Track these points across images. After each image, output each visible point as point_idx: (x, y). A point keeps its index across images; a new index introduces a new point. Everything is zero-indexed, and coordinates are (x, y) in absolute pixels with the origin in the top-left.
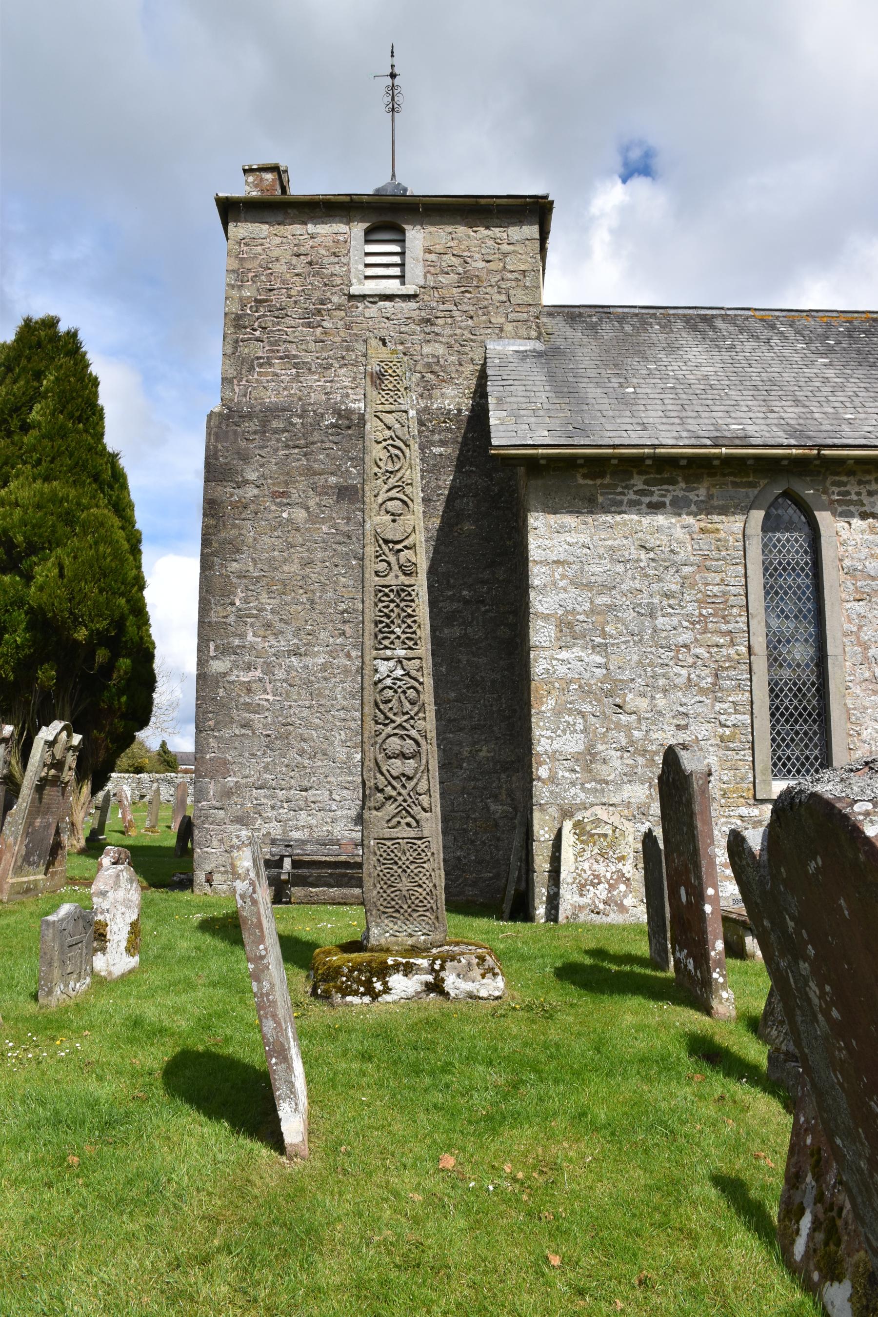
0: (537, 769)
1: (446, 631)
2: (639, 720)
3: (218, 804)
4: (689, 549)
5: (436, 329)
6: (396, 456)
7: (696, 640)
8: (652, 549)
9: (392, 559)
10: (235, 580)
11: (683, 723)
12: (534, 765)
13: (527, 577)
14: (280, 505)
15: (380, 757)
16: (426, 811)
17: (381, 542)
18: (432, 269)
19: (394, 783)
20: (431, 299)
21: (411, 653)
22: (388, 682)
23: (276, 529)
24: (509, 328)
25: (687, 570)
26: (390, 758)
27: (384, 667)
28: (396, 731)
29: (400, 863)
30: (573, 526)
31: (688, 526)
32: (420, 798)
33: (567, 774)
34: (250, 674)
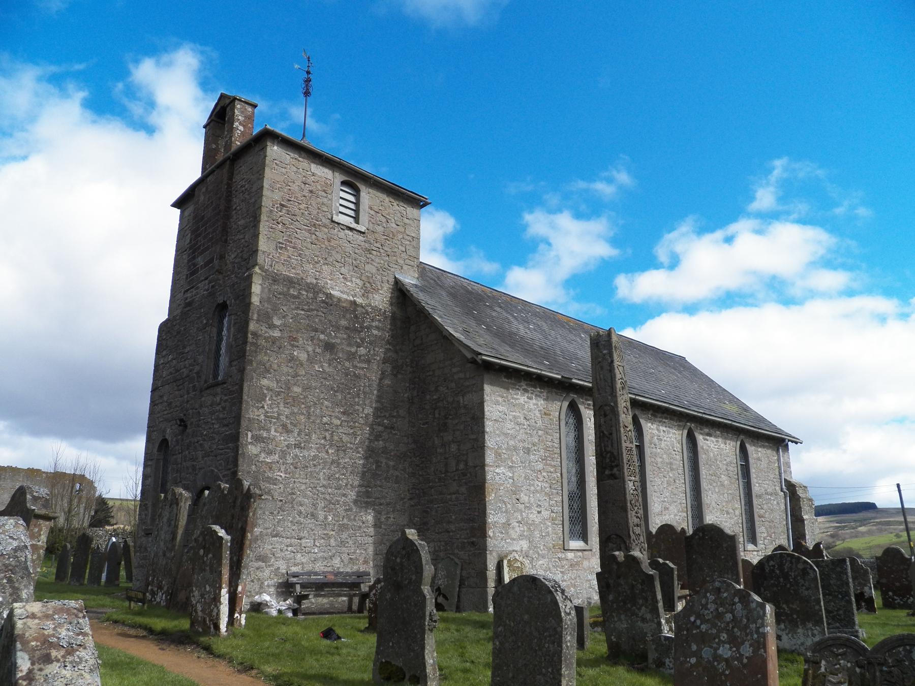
5: (373, 258)
10: (265, 392)
13: (484, 427)
14: (293, 346)
20: (371, 237)
23: (290, 361)
24: (405, 267)
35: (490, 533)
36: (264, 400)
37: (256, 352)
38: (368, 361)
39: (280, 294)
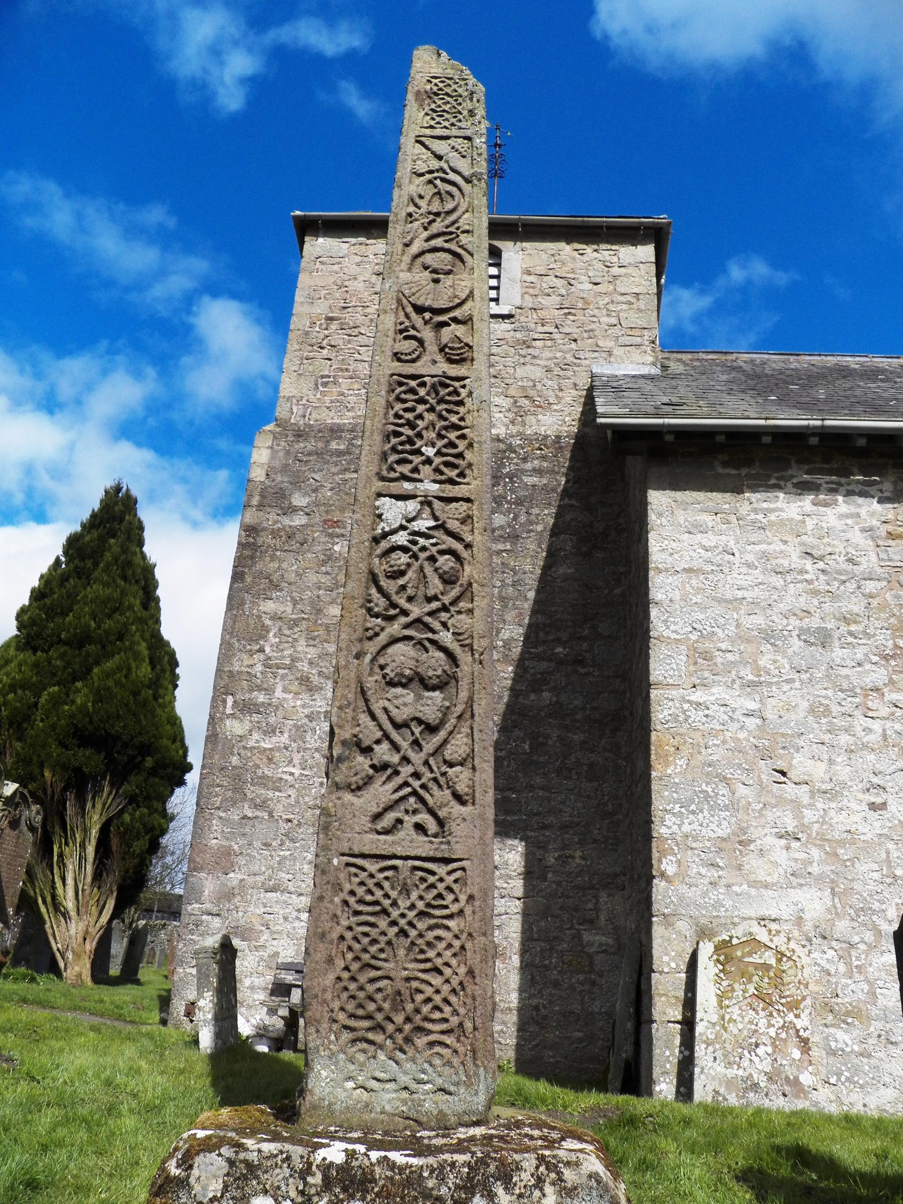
0: (660, 861)
1: (533, 696)
2: (812, 794)
3: (215, 910)
4: (874, 558)
5: (535, 352)
6: (448, 193)
7: (892, 682)
8: (821, 558)
9: (427, 334)
11: (879, 800)
12: (655, 855)
14: (331, 536)
15: (371, 682)
16: (463, 803)
17: (409, 309)
18: (531, 291)
19: (394, 735)
21: (451, 491)
22: (401, 538)
23: (324, 563)
25: (870, 586)
26: (391, 684)
27: (393, 512)
28: (407, 632)
29: (395, 914)
30: (710, 524)
31: (871, 529)
32: (451, 771)
33: (703, 871)
34: (274, 739)
35: (667, 865)
36: (264, 637)
37: (252, 558)
38: (514, 537)
39: (309, 454)
